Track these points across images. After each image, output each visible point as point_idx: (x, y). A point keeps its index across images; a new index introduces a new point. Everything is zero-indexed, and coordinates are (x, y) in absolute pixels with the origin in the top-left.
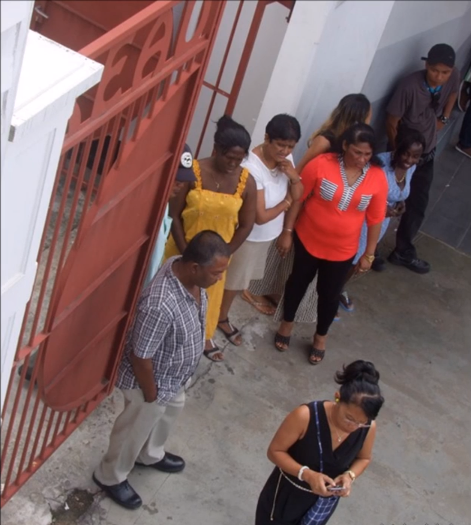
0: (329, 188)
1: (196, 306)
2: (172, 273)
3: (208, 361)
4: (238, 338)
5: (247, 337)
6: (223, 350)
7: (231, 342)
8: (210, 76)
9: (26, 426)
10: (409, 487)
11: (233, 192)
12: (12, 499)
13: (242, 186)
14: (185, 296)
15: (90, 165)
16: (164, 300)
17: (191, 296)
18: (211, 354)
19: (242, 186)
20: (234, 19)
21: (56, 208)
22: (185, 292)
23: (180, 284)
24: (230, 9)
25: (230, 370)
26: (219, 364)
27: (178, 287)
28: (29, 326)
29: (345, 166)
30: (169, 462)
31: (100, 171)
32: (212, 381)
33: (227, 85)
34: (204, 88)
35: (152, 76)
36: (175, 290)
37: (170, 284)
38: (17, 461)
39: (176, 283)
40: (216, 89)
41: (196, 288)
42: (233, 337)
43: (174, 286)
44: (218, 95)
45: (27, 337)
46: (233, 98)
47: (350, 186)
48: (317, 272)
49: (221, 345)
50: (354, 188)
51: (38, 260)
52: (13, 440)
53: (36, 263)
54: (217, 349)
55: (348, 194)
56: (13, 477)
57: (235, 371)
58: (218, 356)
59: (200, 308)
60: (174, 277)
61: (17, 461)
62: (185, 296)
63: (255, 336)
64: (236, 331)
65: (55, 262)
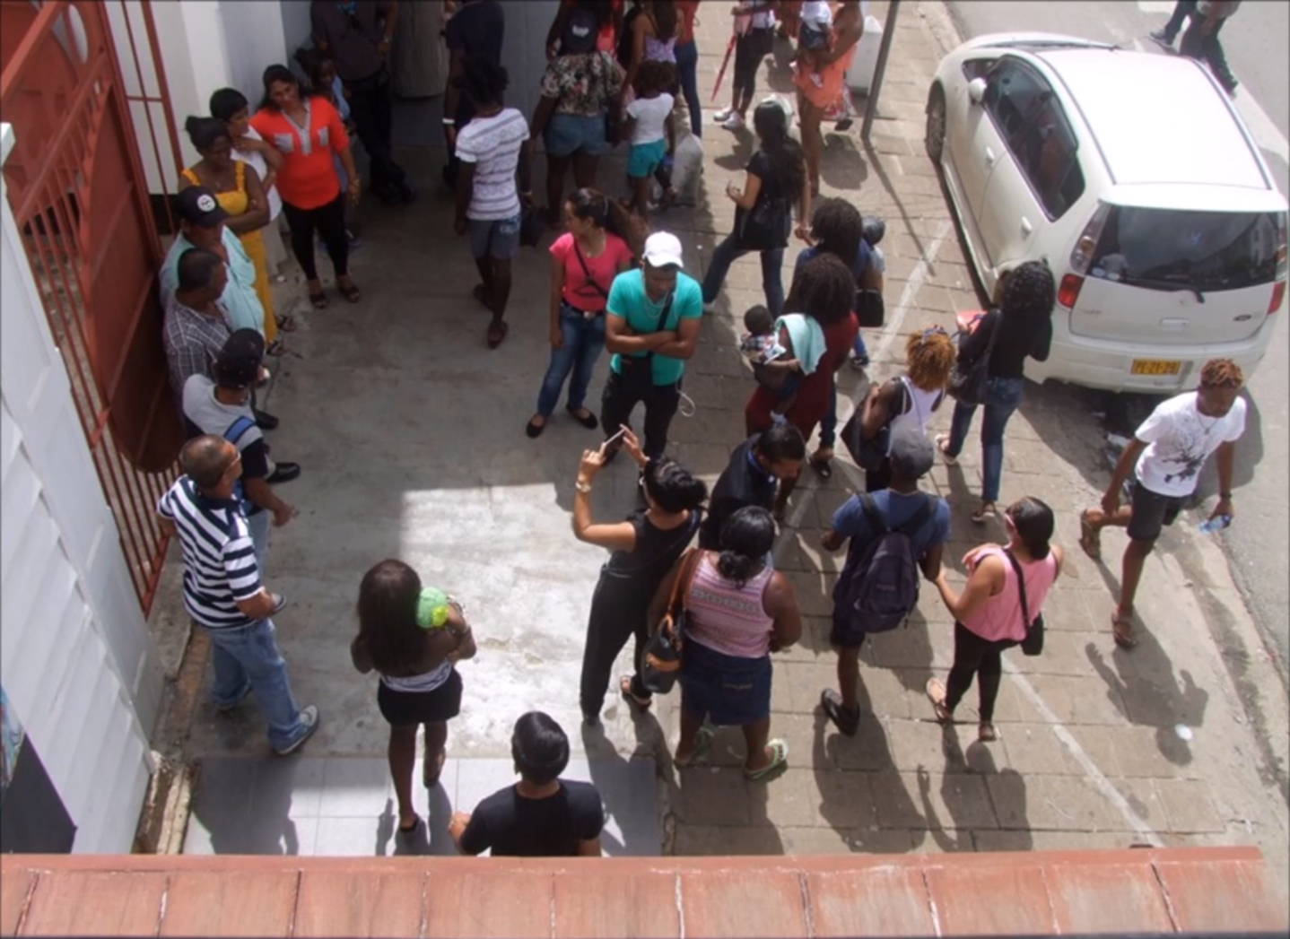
0: (286, 140)
1: (221, 323)
2: (180, 305)
3: (274, 359)
4: (291, 323)
5: (299, 319)
6: (282, 341)
7: (287, 331)
8: (132, 88)
9: (138, 501)
10: (505, 378)
11: (235, 188)
12: (163, 569)
13: (240, 178)
14: (203, 320)
15: (56, 230)
16: (185, 333)
17: (209, 317)
18: (274, 350)
19: (240, 178)
20: (122, 20)
21: (47, 288)
22: (203, 316)
23: (193, 311)
24: (113, 10)
25: (298, 356)
26: (286, 355)
27: (193, 315)
28: (86, 410)
29: (288, 113)
30: (283, 471)
31: (70, 232)
32: (287, 374)
33: (153, 90)
34: (132, 104)
35: (68, 114)
36: (192, 319)
37: (183, 315)
38: (148, 535)
39: (188, 312)
40: (145, 99)
41: (210, 305)
42: (286, 326)
43: (188, 315)
44: (150, 104)
45: (90, 422)
46: (165, 99)
47: (302, 127)
48: (316, 230)
49: (278, 338)
50: (307, 127)
51: (58, 343)
52: (132, 519)
53: (57, 350)
54: (276, 343)
55: (305, 137)
56: (153, 551)
57: (303, 354)
58: (280, 349)
59: (224, 323)
60: (184, 308)
61: (148, 535)
62: (203, 320)
63: (303, 313)
64: (285, 319)
65: (77, 341)
